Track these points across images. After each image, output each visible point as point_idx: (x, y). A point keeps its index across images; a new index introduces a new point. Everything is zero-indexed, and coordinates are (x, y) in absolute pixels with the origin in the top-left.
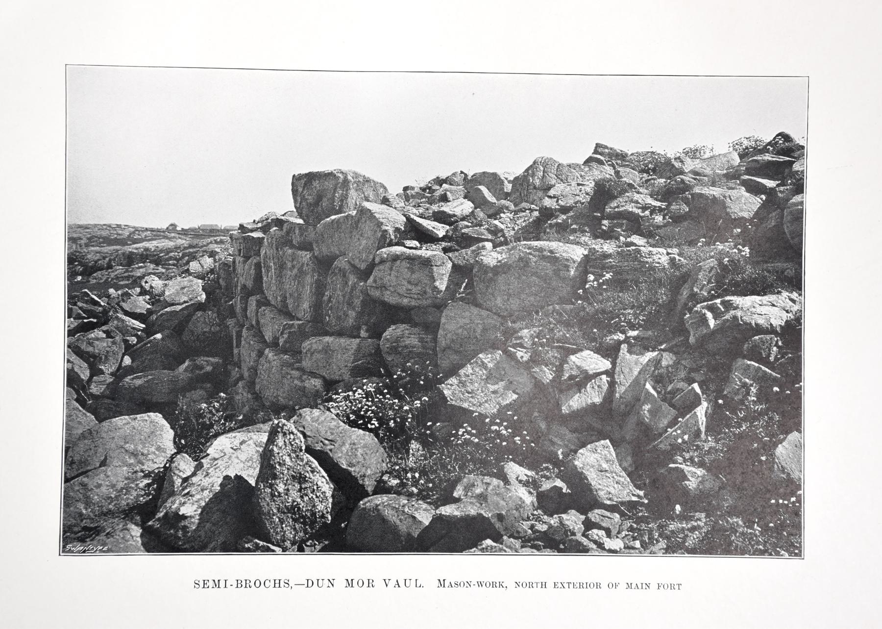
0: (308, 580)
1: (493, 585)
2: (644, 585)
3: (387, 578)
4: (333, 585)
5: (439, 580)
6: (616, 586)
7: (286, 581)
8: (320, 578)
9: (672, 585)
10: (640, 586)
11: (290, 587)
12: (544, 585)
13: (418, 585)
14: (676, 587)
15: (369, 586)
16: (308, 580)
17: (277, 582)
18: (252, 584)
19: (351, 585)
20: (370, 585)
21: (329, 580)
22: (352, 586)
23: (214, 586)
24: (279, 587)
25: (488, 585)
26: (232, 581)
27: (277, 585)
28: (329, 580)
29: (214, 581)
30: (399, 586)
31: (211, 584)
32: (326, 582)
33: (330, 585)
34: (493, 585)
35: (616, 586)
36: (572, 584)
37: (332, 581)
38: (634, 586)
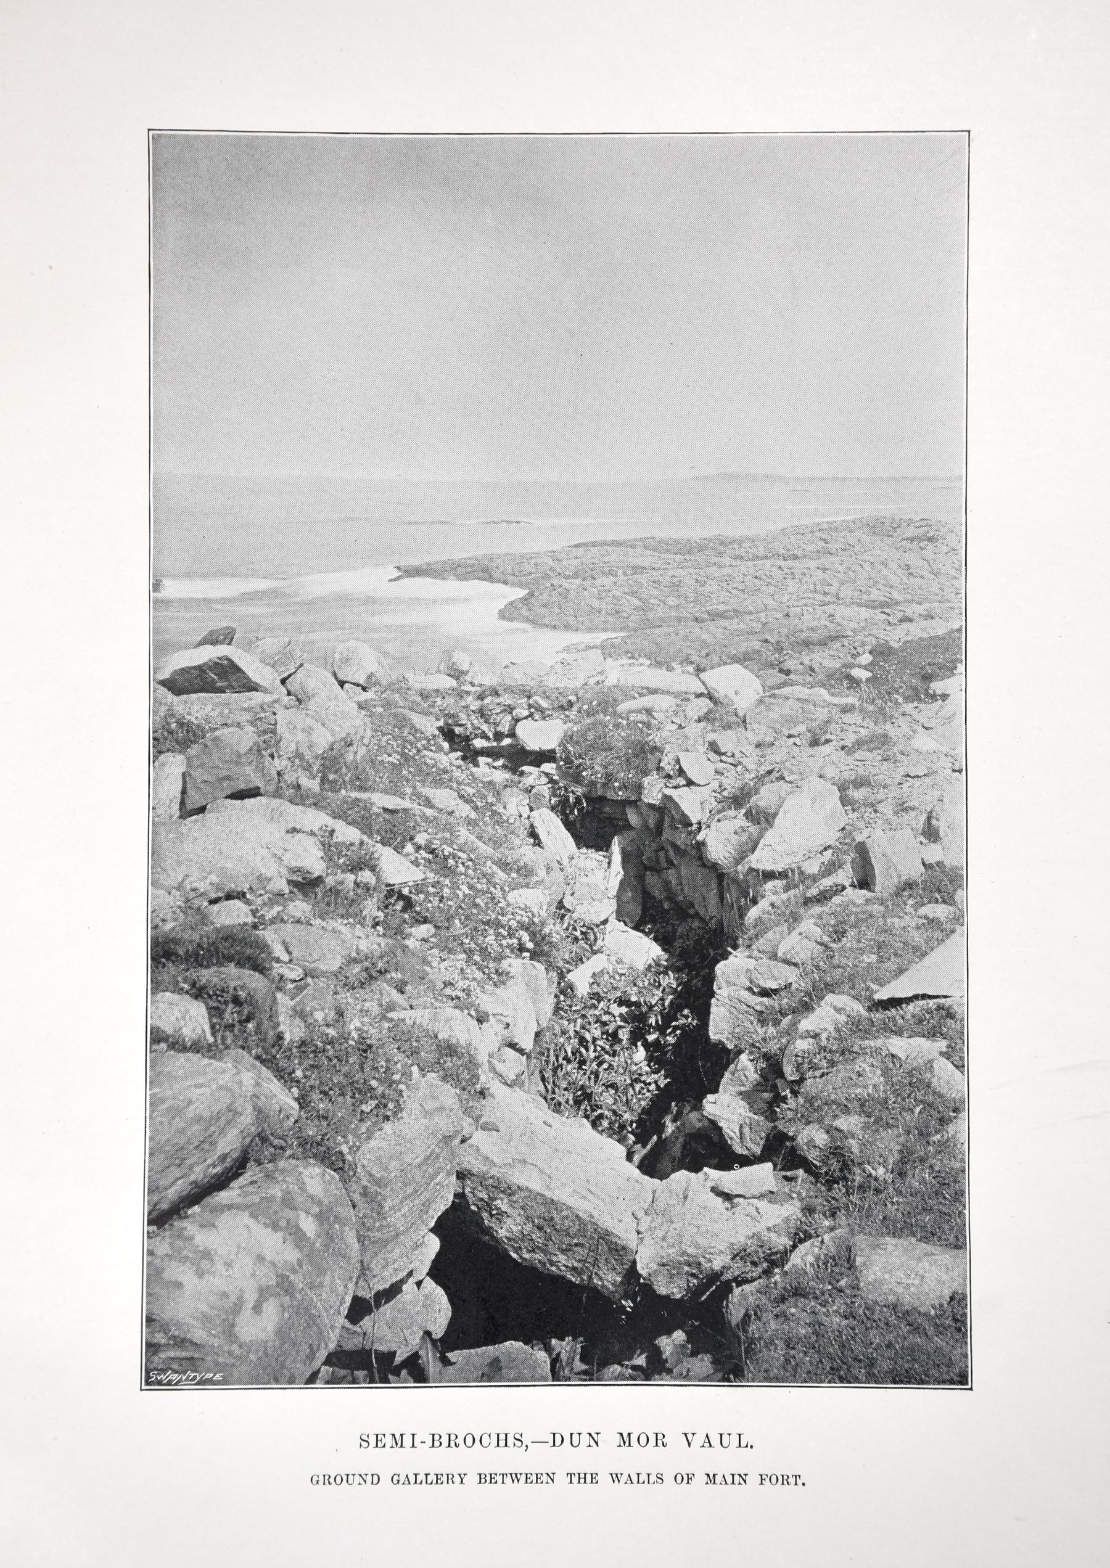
0: (554, 1434)
1: (784, 1480)
2: (737, 1478)
3: (689, 1431)
4: (597, 1443)
5: (621, 1434)
6: (689, 1478)
7: (518, 1437)
8: (575, 1431)
9: (785, 1477)
10: (729, 1480)
11: (524, 1445)
12: (711, 1479)
13: (743, 1444)
14: (457, 1479)
15: (449, 1446)
16: (554, 1434)
17: (502, 1437)
18: (460, 1441)
19: (627, 1444)
20: (660, 1443)
21: (590, 1434)
22: (630, 1445)
23: (394, 1445)
24: (506, 1445)
25: (774, 1479)
26: (424, 1435)
27: (502, 1443)
28: (590, 1434)
29: (394, 1435)
30: (710, 1446)
31: (389, 1440)
32: (585, 1438)
33: (593, 1443)
34: (784, 1480)
35: (689, 1478)
36: (577, 1476)
37: (595, 1436)
38: (719, 1479)
